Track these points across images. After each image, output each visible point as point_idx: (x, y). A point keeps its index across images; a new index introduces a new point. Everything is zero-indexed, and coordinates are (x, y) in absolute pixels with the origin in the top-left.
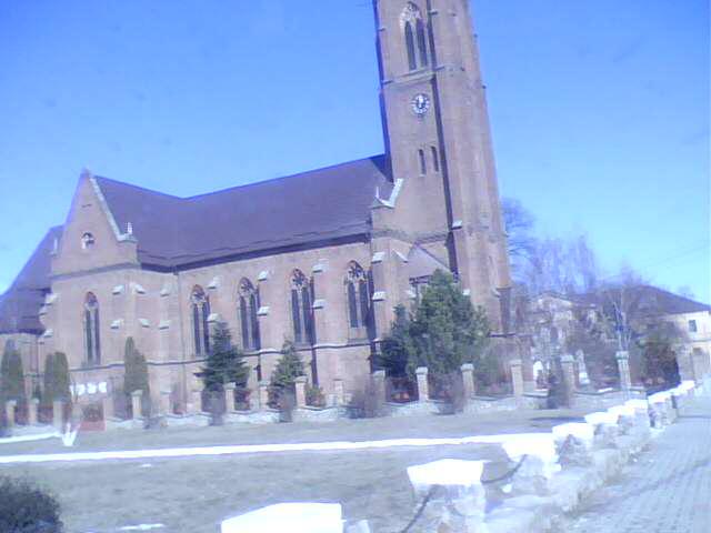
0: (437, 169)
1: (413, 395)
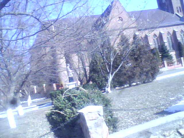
0: (181, 12)
1: (164, 66)
